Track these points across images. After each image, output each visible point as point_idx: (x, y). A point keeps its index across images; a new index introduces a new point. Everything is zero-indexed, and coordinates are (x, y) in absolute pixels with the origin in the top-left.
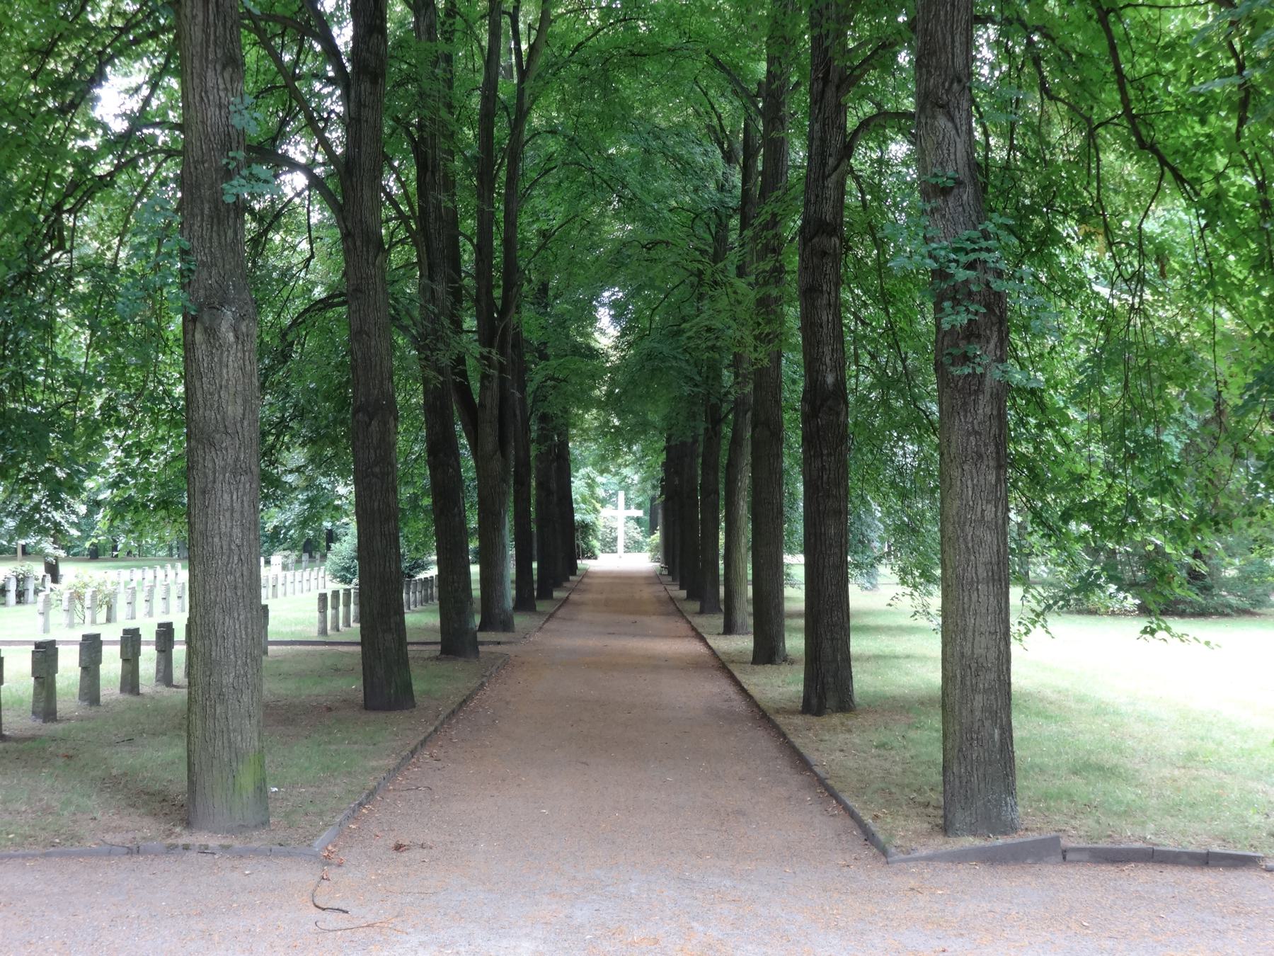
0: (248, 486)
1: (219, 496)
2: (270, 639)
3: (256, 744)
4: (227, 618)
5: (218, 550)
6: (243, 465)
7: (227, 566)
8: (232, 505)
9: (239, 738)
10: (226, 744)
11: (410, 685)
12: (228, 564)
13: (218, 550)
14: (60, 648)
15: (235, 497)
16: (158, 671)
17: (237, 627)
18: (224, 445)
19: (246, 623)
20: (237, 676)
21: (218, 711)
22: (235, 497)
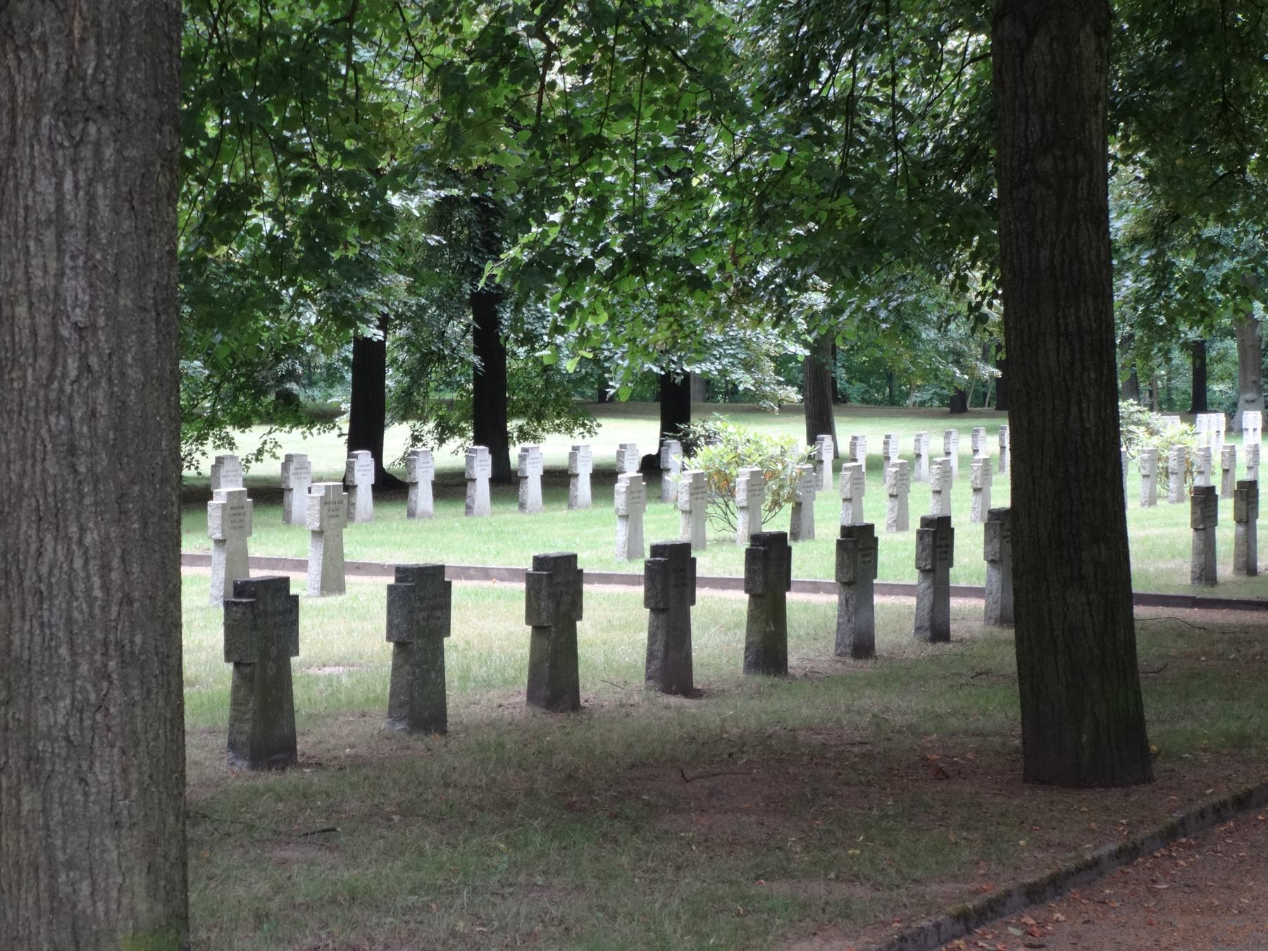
0: (108, 152)
1: (25, 180)
2: (1137, 587)
3: (142, 907)
4: (49, 539)
5: (24, 338)
6: (94, 92)
7: (47, 386)
8: (59, 208)
9: (85, 888)
10: (45, 904)
11: (1138, 724)
12: (51, 378)
13: (24, 338)
14: (460, 589)
15: (68, 186)
16: (651, 655)
17: (78, 563)
18: (36, 34)
19: (104, 554)
20: (77, 709)
21: (26, 808)
22: (68, 186)
